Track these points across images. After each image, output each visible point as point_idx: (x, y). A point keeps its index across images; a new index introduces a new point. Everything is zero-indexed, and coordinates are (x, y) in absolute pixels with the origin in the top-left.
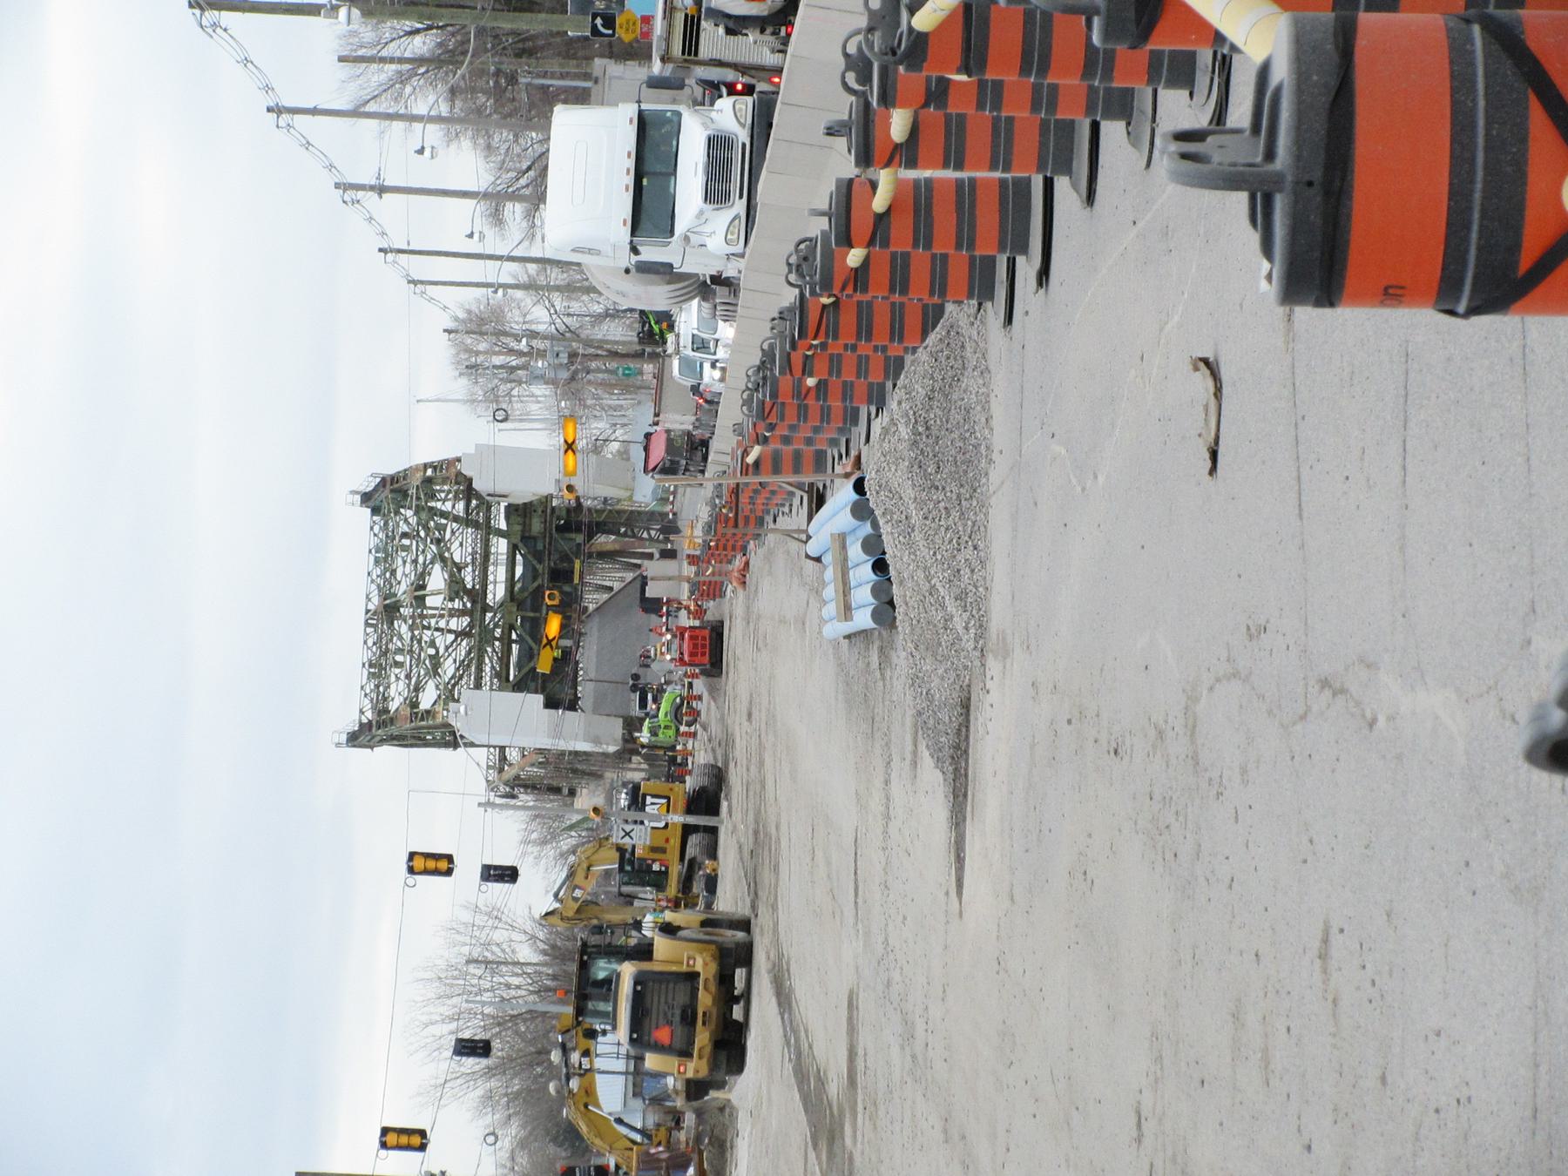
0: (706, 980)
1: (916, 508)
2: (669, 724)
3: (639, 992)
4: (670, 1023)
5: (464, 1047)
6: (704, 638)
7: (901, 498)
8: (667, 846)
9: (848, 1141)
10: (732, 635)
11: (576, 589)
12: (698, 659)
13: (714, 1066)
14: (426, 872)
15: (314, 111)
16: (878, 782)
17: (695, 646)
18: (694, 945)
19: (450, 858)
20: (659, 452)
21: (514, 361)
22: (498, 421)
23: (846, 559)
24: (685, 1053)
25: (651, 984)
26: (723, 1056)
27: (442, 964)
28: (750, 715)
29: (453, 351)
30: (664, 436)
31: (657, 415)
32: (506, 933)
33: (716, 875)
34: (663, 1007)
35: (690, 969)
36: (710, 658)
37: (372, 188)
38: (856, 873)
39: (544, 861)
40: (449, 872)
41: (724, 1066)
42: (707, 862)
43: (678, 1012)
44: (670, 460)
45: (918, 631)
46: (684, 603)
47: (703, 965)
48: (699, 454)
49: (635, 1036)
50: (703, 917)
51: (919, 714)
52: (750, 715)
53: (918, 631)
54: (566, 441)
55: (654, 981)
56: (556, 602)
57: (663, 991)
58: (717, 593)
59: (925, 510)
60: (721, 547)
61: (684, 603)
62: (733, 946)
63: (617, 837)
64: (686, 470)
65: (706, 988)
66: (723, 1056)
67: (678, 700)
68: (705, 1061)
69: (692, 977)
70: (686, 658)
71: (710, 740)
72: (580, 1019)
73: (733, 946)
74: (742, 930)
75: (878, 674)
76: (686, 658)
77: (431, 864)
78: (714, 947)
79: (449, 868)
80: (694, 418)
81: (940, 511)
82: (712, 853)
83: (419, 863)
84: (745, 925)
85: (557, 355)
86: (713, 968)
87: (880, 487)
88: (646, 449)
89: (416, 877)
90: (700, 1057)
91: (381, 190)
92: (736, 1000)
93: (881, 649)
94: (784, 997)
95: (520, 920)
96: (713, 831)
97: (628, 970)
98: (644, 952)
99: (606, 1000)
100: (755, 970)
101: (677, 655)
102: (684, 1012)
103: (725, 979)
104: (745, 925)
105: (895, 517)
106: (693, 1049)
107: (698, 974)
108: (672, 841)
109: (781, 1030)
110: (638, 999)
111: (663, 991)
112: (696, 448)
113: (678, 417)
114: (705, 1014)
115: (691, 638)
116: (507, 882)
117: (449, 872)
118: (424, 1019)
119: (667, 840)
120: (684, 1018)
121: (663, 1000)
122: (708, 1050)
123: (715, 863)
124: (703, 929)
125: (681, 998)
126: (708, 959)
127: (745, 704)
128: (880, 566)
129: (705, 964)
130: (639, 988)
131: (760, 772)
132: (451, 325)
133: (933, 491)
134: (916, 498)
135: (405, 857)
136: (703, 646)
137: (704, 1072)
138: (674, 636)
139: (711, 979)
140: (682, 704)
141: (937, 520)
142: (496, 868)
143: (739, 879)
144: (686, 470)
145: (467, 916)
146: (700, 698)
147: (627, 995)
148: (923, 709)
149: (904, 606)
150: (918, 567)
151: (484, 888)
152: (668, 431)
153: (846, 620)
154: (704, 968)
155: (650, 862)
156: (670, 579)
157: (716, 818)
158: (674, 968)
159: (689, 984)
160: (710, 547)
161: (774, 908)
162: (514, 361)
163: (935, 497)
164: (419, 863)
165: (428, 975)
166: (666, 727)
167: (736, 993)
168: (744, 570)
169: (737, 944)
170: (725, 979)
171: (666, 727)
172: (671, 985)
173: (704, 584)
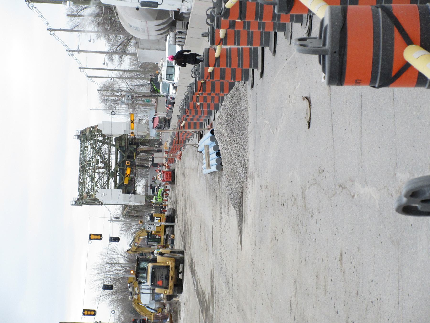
0: (172, 268)
2: (160, 197)
5: (105, 287)
6: (170, 174)
7: (224, 135)
8: (160, 231)
9: (211, 311)
10: (178, 173)
11: (134, 161)
12: (168, 180)
13: (174, 291)
14: (94, 239)
15: (60, 30)
17: (167, 176)
19: (101, 235)
20: (157, 123)
21: (117, 98)
22: (112, 115)
23: (209, 152)
24: (166, 288)
25: (156, 269)
28: (183, 195)
29: (100, 96)
30: (158, 118)
31: (156, 113)
33: (174, 239)
34: (160, 275)
35: (167, 265)
37: (77, 51)
38: (212, 238)
39: (127, 235)
40: (101, 239)
41: (177, 291)
42: (171, 235)
43: (164, 277)
45: (229, 171)
46: (164, 164)
47: (171, 263)
48: (168, 123)
49: (152, 283)
50: (171, 250)
51: (230, 194)
52: (183, 195)
53: (229, 171)
54: (131, 120)
56: (129, 164)
58: (173, 161)
63: (147, 229)
64: (164, 127)
65: (172, 270)
67: (163, 191)
68: (172, 290)
69: (168, 267)
70: (165, 179)
72: (137, 279)
73: (179, 258)
74: (181, 254)
75: (218, 183)
76: (165, 179)
77: (96, 237)
78: (174, 259)
79: (101, 238)
80: (166, 113)
81: (234, 139)
82: (173, 233)
83: (92, 237)
84: (182, 252)
86: (174, 264)
88: (153, 122)
89: (92, 240)
90: (170, 289)
91: (79, 51)
92: (180, 273)
93: (219, 177)
94: (193, 272)
95: (120, 252)
96: (173, 227)
97: (150, 265)
98: (155, 260)
99: (144, 273)
100: (185, 265)
104: (182, 252)
105: (222, 140)
106: (168, 287)
107: (169, 266)
108: (162, 230)
109: (192, 281)
110: (153, 273)
112: (167, 122)
114: (171, 277)
115: (167, 174)
116: (117, 241)
117: (101, 239)
119: (160, 229)
120: (166, 278)
122: (173, 287)
123: (174, 236)
125: (165, 273)
126: (172, 262)
127: (181, 193)
128: (218, 154)
129: (171, 263)
130: (153, 270)
131: (186, 210)
132: (99, 88)
133: (232, 133)
134: (228, 135)
135: (89, 235)
137: (171, 293)
138: (162, 173)
139: (173, 267)
141: (233, 141)
142: (114, 238)
143: (180, 240)
144: (164, 127)
145: (106, 251)
146: (169, 190)
147: (150, 272)
150: (228, 154)
151: (110, 243)
152: (159, 117)
155: (156, 235)
156: (160, 158)
158: (163, 265)
159: (167, 269)
160: (171, 149)
161: (190, 248)
162: (117, 98)
163: (233, 135)
164: (92, 237)
165: (95, 267)
166: (160, 198)
167: (180, 271)
168: (180, 155)
169: (180, 258)
170: (177, 267)
171: (160, 198)
172: (162, 269)
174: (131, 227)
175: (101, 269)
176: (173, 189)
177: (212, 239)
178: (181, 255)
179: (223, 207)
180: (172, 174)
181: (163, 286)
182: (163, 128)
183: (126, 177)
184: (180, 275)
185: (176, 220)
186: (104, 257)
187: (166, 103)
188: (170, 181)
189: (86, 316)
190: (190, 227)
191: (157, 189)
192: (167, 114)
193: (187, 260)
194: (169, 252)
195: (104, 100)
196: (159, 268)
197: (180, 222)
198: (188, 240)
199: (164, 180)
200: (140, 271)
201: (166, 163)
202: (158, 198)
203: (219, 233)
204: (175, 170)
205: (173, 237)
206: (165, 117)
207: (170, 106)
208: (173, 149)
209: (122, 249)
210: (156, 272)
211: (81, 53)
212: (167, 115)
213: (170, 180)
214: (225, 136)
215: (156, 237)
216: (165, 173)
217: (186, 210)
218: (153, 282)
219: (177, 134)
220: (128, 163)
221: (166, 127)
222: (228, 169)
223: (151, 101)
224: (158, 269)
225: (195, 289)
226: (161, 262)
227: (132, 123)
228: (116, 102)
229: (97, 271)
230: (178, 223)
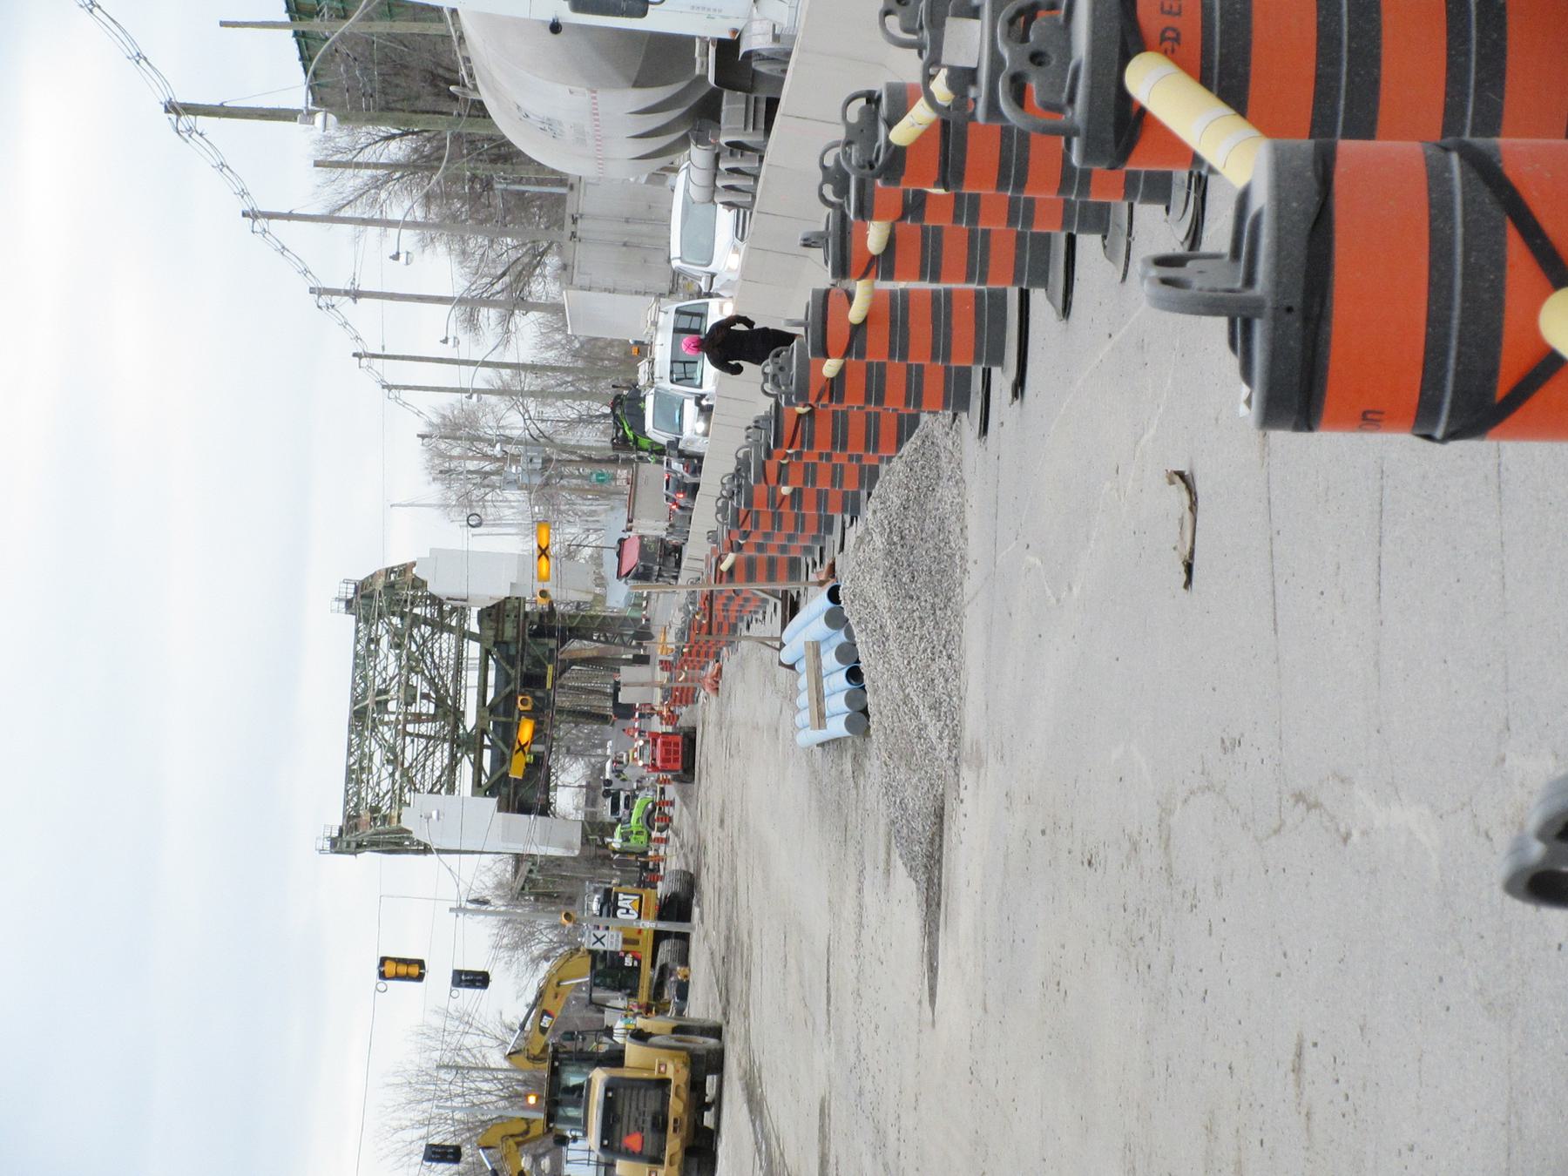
0: (677, 1087)
2: (640, 829)
3: (610, 1098)
6: (676, 744)
7: (876, 607)
11: (549, 695)
12: (669, 766)
14: (398, 977)
15: (290, 216)
16: (851, 890)
17: (667, 752)
19: (421, 963)
20: (632, 557)
23: (819, 668)
25: (622, 1090)
26: (694, 1162)
28: (722, 822)
29: (427, 456)
30: (637, 542)
31: (630, 521)
32: (477, 1039)
33: (688, 981)
34: (634, 1113)
36: (683, 764)
37: (347, 293)
38: (828, 981)
39: (515, 966)
40: (420, 978)
42: (678, 968)
43: (649, 1119)
44: (643, 566)
45: (892, 739)
46: (657, 708)
47: (675, 1072)
48: (673, 559)
49: (606, 1142)
50: (674, 1024)
51: (893, 823)
52: (722, 822)
53: (892, 739)
55: (625, 1089)
56: (528, 707)
57: (634, 1097)
59: (900, 619)
60: (694, 652)
61: (657, 708)
62: (705, 1052)
64: (660, 575)
65: (677, 1094)
66: (694, 1162)
67: (650, 806)
69: (664, 1083)
70: (659, 763)
71: (682, 846)
72: (551, 1125)
73: (705, 1052)
74: (713, 1037)
76: (659, 763)
77: (402, 970)
78: (684, 1054)
79: (420, 973)
80: (667, 524)
83: (390, 968)
84: (716, 1032)
87: (854, 596)
88: (620, 555)
89: (388, 982)
90: (671, 1164)
91: (356, 295)
92: (708, 1107)
93: (855, 757)
96: (684, 938)
98: (615, 1058)
99: (576, 1105)
101: (649, 762)
102: (655, 1118)
103: (697, 1086)
104: (716, 1032)
105: (870, 626)
106: (664, 1155)
107: (668, 1081)
109: (752, 1136)
110: (609, 1106)
111: (634, 1097)
112: (670, 554)
113: (652, 523)
114: (675, 1121)
115: (664, 743)
117: (420, 978)
118: (395, 1124)
120: (654, 1125)
122: (679, 1157)
124: (675, 1036)
125: (652, 1105)
126: (680, 1066)
128: (854, 675)
131: (732, 879)
132: (425, 430)
134: (890, 608)
135: (377, 962)
139: (683, 1086)
140: (654, 810)
142: (467, 973)
144: (660, 575)
145: (437, 1022)
146: (672, 804)
149: (878, 715)
150: (892, 676)
151: (455, 993)
152: (641, 537)
153: (820, 728)
154: (675, 1074)
155: (622, 954)
156: (642, 685)
157: (687, 924)
158: (645, 1075)
160: (683, 654)
161: (746, 1015)
164: (390, 968)
165: (398, 1080)
167: (707, 1099)
169: (709, 1051)
170: (697, 1086)
171: (637, 833)
173: (677, 690)
174: (532, 934)
175: (418, 1086)
178: (712, 1042)
179: (869, 867)
180: (683, 744)
181: (644, 1153)
182: (654, 578)
183: (517, 752)
184: (706, 1113)
185: (696, 911)
187: (667, 488)
188: (677, 771)
191: (627, 798)
192: (671, 526)
193: (735, 1061)
194: (670, 1030)
195: (441, 472)
196: (632, 1088)
197: (709, 921)
198: (738, 989)
199: (654, 767)
200: (560, 1096)
201: (662, 704)
202: (632, 832)
203: (853, 961)
204: (695, 729)
205: (686, 976)
206: (664, 536)
207: (681, 496)
208: (690, 653)
211: (361, 301)
212: (670, 530)
213: (679, 765)
216: (659, 741)
217: (732, 879)
219: (706, 599)
220: (524, 702)
224: (628, 1092)
226: (637, 1065)
227: (543, 557)
228: (485, 478)
229: (403, 1095)
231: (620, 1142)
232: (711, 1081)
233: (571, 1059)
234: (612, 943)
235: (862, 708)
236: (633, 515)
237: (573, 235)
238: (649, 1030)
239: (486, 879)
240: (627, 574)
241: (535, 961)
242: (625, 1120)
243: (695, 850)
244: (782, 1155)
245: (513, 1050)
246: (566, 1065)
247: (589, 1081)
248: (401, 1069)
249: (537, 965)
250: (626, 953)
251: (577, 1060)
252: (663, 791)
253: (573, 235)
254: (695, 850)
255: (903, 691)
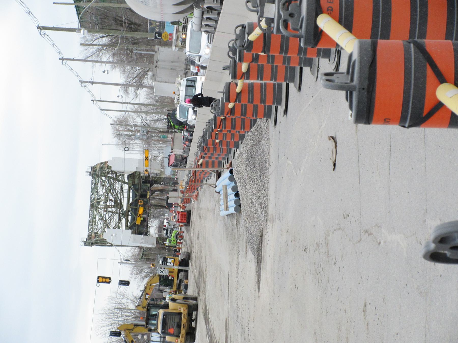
0: (184, 315)
1: (248, 178)
2: (174, 240)
4: (173, 327)
6: (185, 215)
7: (243, 175)
8: (174, 271)
11: (148, 200)
12: (183, 221)
14: (103, 282)
15: (73, 60)
16: (235, 258)
17: (182, 217)
18: (181, 305)
19: (110, 278)
20: (172, 160)
21: (130, 133)
23: (227, 193)
24: (178, 336)
25: (168, 316)
26: (189, 337)
27: (107, 309)
28: (198, 238)
29: (113, 130)
30: (174, 156)
31: (172, 150)
32: (126, 300)
33: (188, 284)
34: (171, 323)
37: (90, 82)
38: (229, 279)
39: (137, 279)
40: (109, 282)
41: (189, 340)
42: (185, 280)
43: (176, 324)
45: (248, 214)
46: (179, 204)
47: (183, 310)
48: (184, 161)
51: (248, 238)
52: (198, 238)
53: (248, 214)
54: (145, 157)
56: (142, 204)
58: (189, 202)
59: (250, 179)
63: (159, 273)
64: (181, 166)
65: (184, 317)
66: (189, 337)
67: (177, 233)
69: (180, 314)
70: (180, 221)
72: (147, 326)
73: (192, 305)
74: (195, 300)
75: (236, 226)
76: (180, 221)
77: (104, 280)
78: (186, 305)
80: (183, 151)
81: (254, 179)
82: (187, 278)
83: (100, 280)
84: (196, 299)
85: (143, 132)
86: (186, 311)
87: (237, 172)
88: (169, 159)
89: (100, 284)
90: (182, 337)
91: (92, 83)
92: (193, 321)
93: (237, 219)
94: (207, 320)
96: (187, 271)
98: (166, 306)
99: (155, 320)
100: (198, 312)
102: (177, 324)
104: (196, 299)
106: (180, 335)
107: (182, 313)
109: (206, 330)
110: (164, 320)
112: (184, 159)
113: (178, 150)
114: (184, 325)
115: (181, 215)
117: (109, 282)
118: (101, 325)
120: (177, 326)
121: (171, 319)
122: (184, 335)
123: (187, 281)
125: (177, 320)
126: (185, 309)
128: (237, 195)
129: (184, 310)
132: (112, 122)
134: (247, 176)
135: (97, 278)
136: (185, 217)
138: (176, 214)
139: (186, 314)
140: (178, 234)
141: (254, 182)
142: (123, 281)
143: (194, 286)
144: (181, 166)
145: (114, 295)
146: (183, 232)
148: (249, 237)
149: (244, 207)
150: (248, 195)
151: (119, 287)
152: (175, 154)
153: (227, 210)
158: (175, 311)
160: (187, 189)
161: (204, 294)
162: (130, 133)
163: (253, 175)
164: (100, 280)
165: (103, 312)
166: (174, 241)
167: (193, 319)
168: (197, 195)
170: (190, 314)
171: (174, 241)
174: (142, 270)
176: (187, 231)
177: (228, 285)
178: (194, 302)
182: (179, 166)
183: (138, 217)
185: (190, 264)
186: (113, 302)
187: (183, 140)
188: (185, 223)
189: (100, 284)
190: (204, 272)
192: (184, 151)
193: (201, 307)
195: (117, 135)
196: (171, 315)
197: (194, 266)
198: (202, 286)
200: (150, 317)
201: (181, 203)
203: (236, 278)
208: (189, 188)
209: (132, 294)
210: (167, 319)
212: (184, 152)
213: (186, 221)
214: (245, 176)
215: (169, 277)
216: (180, 214)
218: (164, 330)
220: (140, 202)
221: (182, 165)
222: (247, 212)
223: (168, 137)
224: (170, 316)
225: (208, 338)
226: (172, 308)
230: (192, 267)
231: (167, 331)
232: (194, 313)
233: (153, 306)
234: (165, 273)
235: (239, 205)
236: (173, 148)
237: (156, 66)
238: (176, 298)
239: (129, 254)
240: (171, 165)
241: (143, 278)
242: (169, 325)
243: (190, 246)
244: (214, 335)
245: (138, 305)
246: (152, 308)
247: (158, 313)
248: (104, 309)
249: (144, 279)
250: (170, 275)
251: (155, 307)
252: (181, 229)
253: (156, 66)
254: (190, 246)
255: (251, 200)
